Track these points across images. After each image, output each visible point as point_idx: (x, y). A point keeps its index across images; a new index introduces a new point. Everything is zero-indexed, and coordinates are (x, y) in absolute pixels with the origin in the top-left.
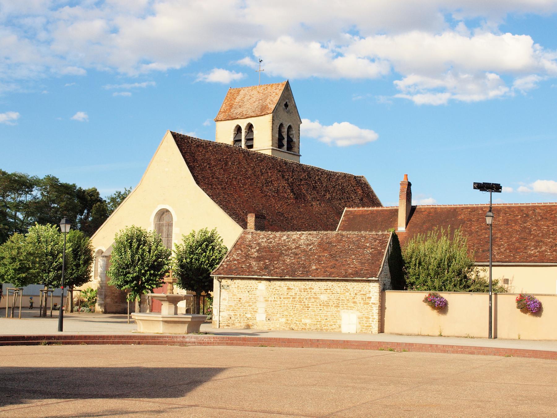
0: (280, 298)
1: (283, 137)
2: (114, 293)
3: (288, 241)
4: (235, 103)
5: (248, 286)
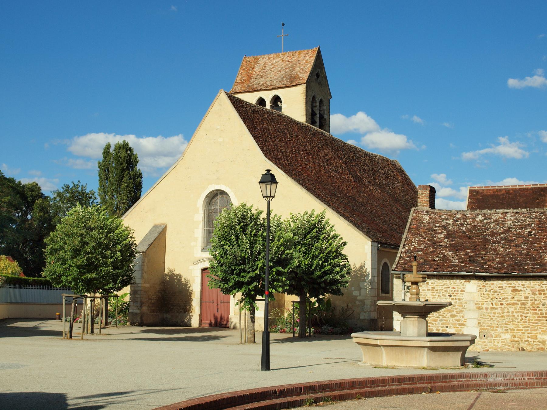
0: (502, 304)
1: (315, 113)
2: (152, 300)
3: (487, 223)
4: (254, 73)
5: (449, 288)
